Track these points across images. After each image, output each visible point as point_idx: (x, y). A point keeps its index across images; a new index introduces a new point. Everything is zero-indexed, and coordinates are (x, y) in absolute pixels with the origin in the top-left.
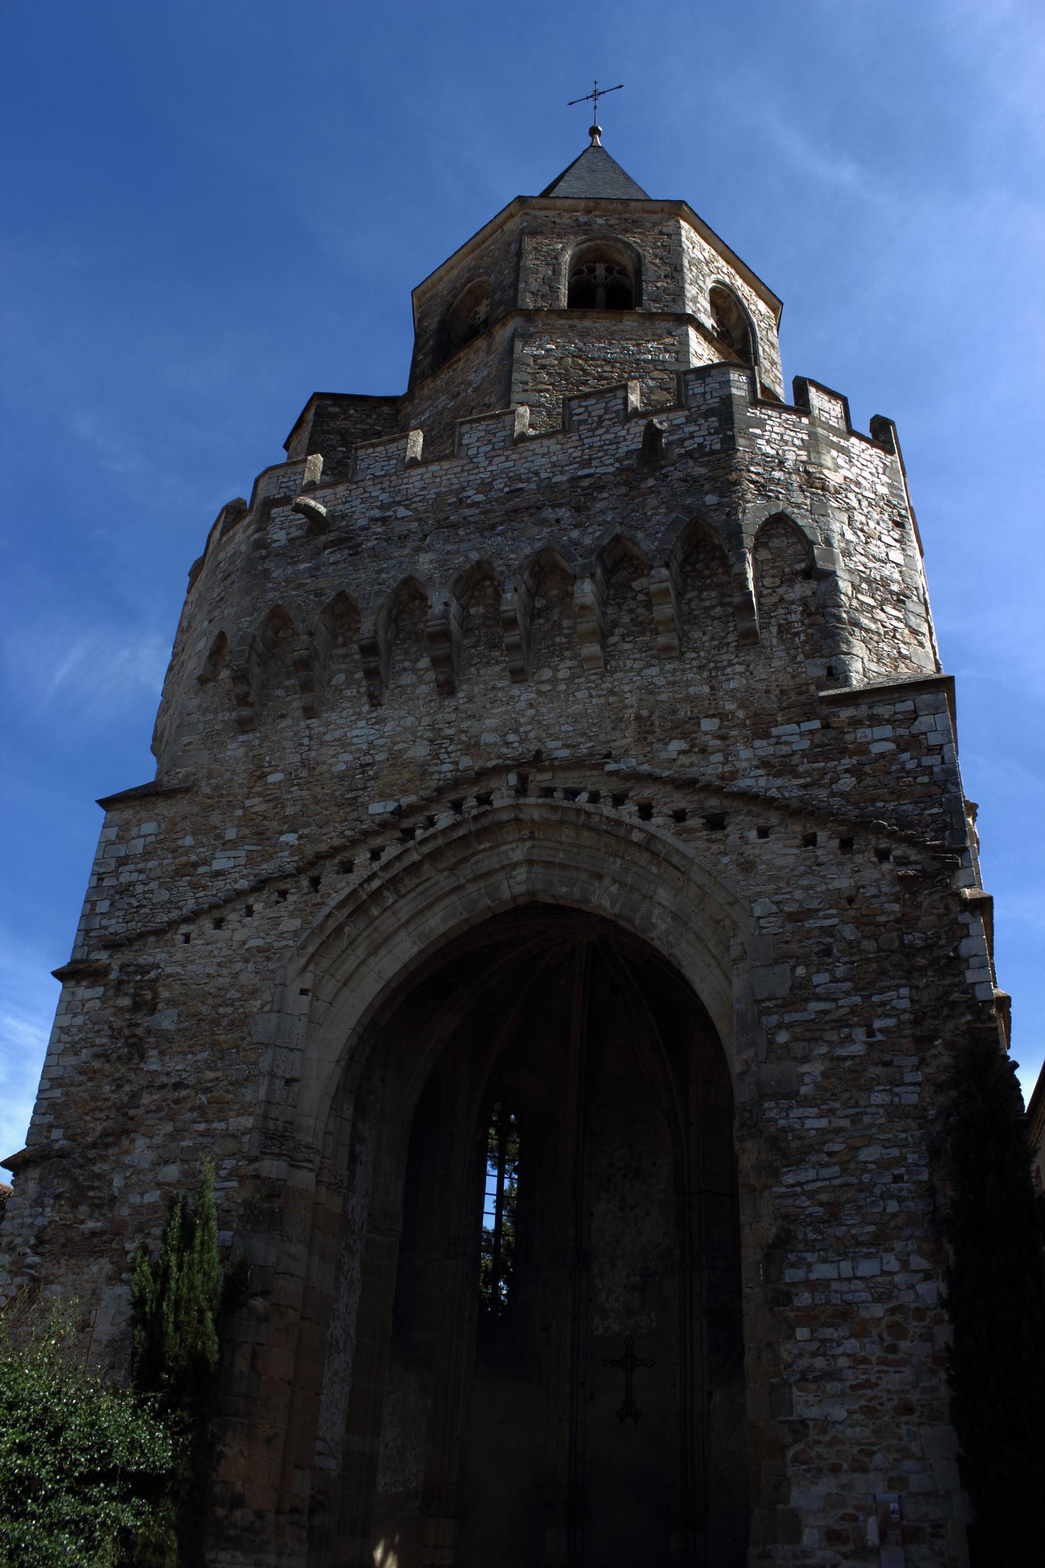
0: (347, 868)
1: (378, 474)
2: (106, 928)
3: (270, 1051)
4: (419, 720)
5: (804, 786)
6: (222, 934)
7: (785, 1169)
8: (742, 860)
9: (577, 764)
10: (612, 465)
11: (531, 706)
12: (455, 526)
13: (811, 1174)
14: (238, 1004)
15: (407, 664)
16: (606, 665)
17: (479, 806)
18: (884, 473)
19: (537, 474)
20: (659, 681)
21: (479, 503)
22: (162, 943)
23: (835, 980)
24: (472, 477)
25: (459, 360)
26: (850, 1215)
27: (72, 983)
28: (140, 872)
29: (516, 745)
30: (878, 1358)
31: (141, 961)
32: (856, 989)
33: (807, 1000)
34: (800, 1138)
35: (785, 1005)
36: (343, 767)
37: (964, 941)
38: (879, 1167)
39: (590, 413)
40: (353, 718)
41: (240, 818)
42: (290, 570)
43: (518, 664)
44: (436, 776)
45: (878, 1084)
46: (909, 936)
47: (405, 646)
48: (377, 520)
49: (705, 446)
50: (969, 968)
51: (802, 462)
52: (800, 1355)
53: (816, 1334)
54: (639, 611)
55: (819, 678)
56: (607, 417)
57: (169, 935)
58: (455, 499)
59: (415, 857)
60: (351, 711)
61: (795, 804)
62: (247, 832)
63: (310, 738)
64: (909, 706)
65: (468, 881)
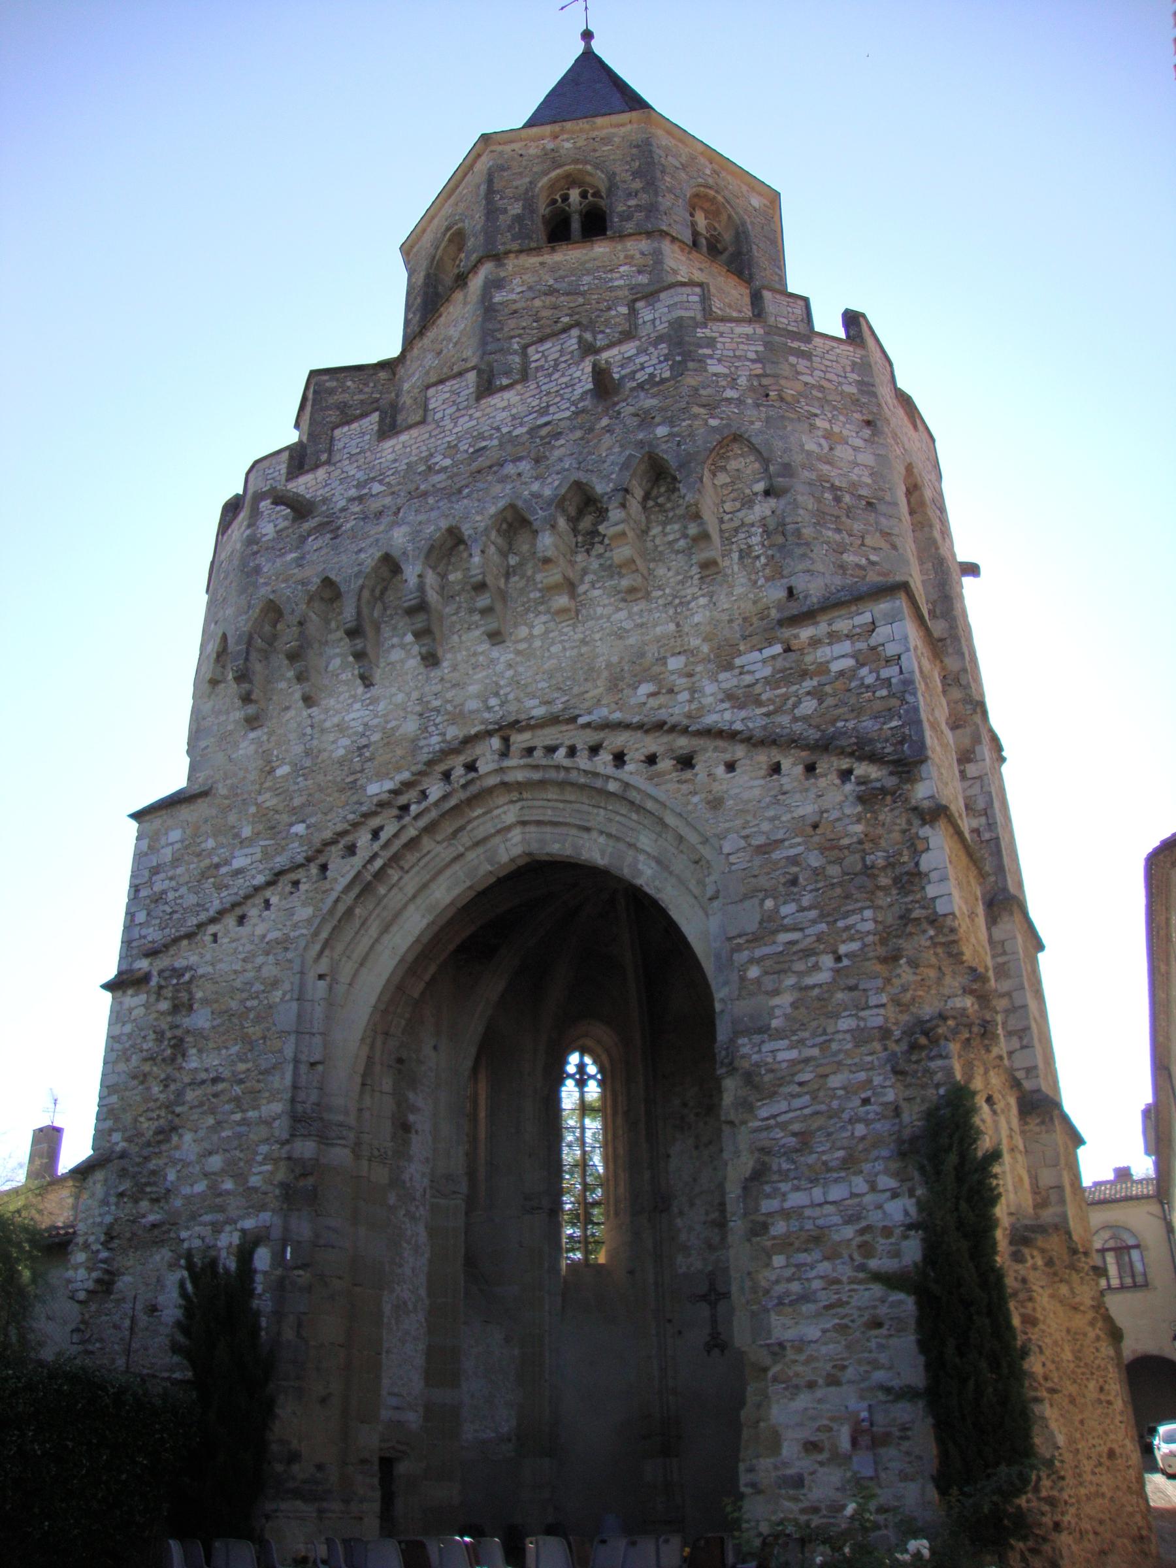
0: (351, 850)
1: (354, 452)
2: (145, 937)
4: (408, 695)
5: (767, 715)
6: (244, 931)
7: (759, 1104)
8: (711, 797)
9: (554, 720)
10: (568, 409)
11: (510, 666)
12: (425, 494)
13: (783, 1106)
14: (262, 996)
15: (395, 640)
16: (577, 615)
18: (853, 371)
19: (498, 429)
20: (628, 625)
21: (446, 468)
22: (194, 946)
23: (802, 909)
24: (440, 442)
25: (440, 316)
26: (820, 1142)
27: (119, 993)
28: (171, 879)
30: (849, 1277)
31: (177, 965)
32: (822, 916)
33: (775, 932)
34: (772, 1071)
35: (756, 939)
36: (341, 752)
37: (924, 856)
38: (848, 1092)
39: (546, 357)
41: (254, 815)
42: (279, 562)
43: (494, 626)
44: (426, 750)
45: (845, 1010)
46: (872, 857)
47: (393, 622)
49: (655, 376)
50: (929, 882)
51: (757, 376)
52: (777, 1282)
55: (780, 600)
56: (563, 359)
57: (199, 937)
58: (424, 468)
59: (412, 832)
60: (347, 695)
61: (759, 734)
62: (261, 827)
63: (312, 726)
64: (866, 618)
65: (467, 849)
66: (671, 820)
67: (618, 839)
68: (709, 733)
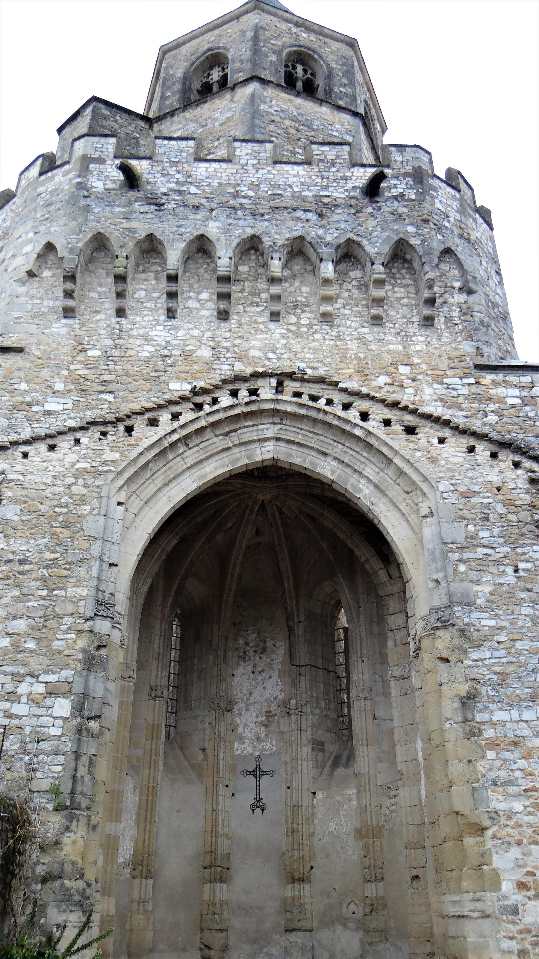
0: (153, 423)
3: (99, 542)
5: (466, 417)
8: (429, 456)
9: (321, 381)
13: (488, 654)
15: (192, 294)
17: (250, 395)
20: (370, 337)
29: (275, 361)
34: (479, 631)
36: (148, 355)
40: (153, 323)
41: (66, 377)
43: (275, 308)
48: (174, 191)
53: (500, 756)
54: (354, 291)
57: (10, 451)
59: (203, 423)
65: (235, 445)
66: (397, 461)
67: (347, 465)
68: (429, 417)
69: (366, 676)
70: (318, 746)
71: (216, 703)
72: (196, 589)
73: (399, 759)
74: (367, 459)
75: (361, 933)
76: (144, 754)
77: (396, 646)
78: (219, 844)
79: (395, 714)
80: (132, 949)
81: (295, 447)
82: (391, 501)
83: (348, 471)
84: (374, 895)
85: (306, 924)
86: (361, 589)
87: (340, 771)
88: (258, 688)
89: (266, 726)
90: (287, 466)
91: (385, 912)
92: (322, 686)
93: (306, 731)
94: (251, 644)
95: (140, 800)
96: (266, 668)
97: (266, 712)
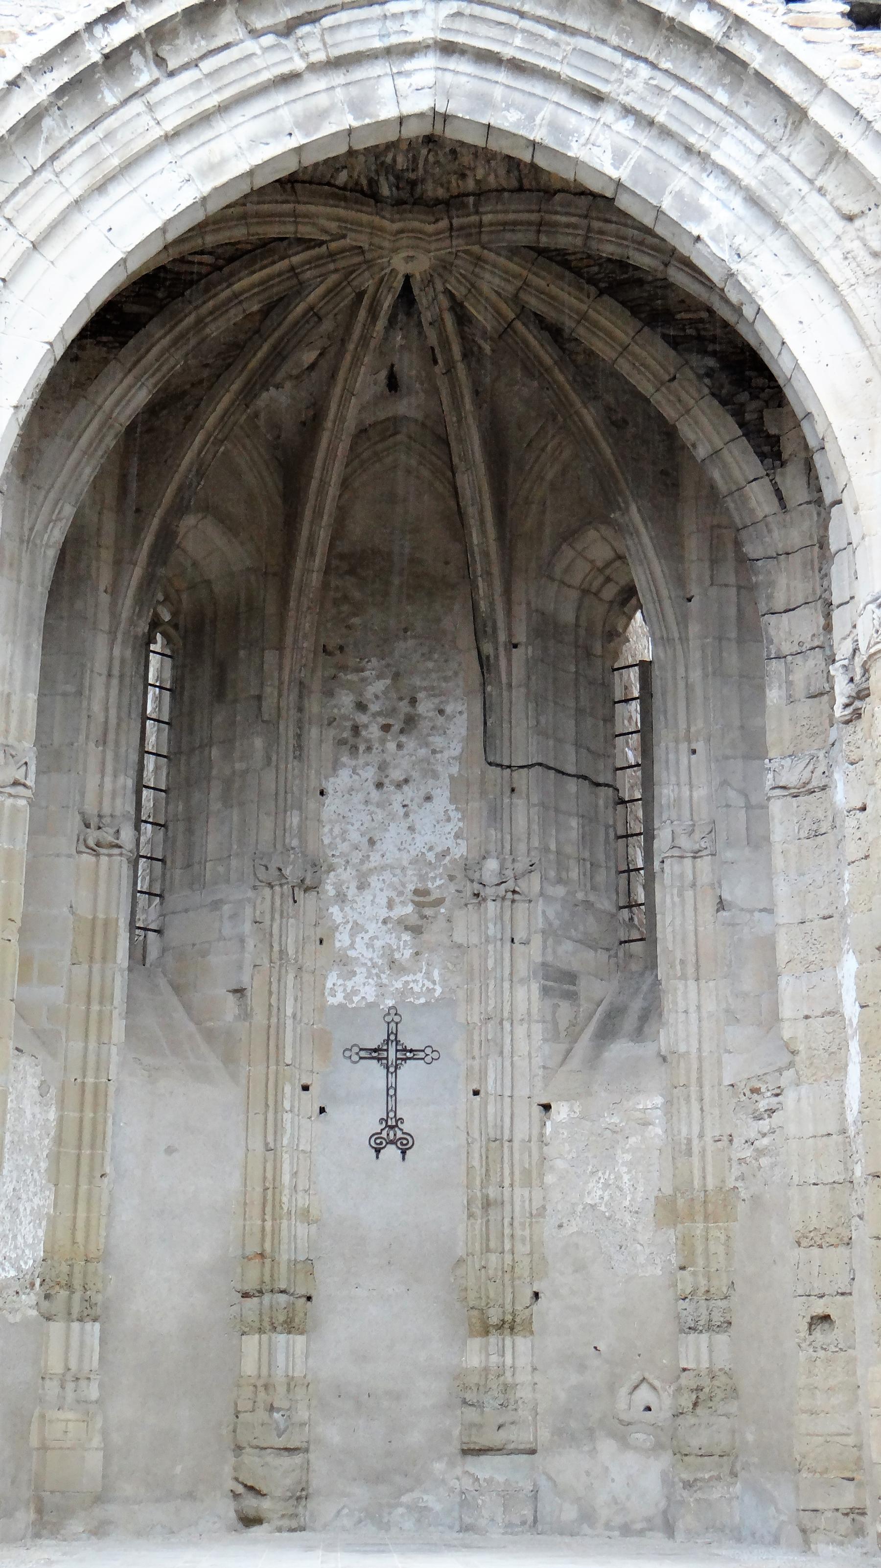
66: (821, 112)
67: (665, 133)
69: (700, 793)
70: (560, 983)
71: (273, 866)
72: (211, 549)
73: (787, 1011)
74: (727, 111)
75: (665, 1460)
76: (69, 1001)
77: (791, 700)
78: (284, 1233)
79: (782, 889)
80: (46, 1495)
81: (502, 76)
82: (798, 246)
83: (668, 151)
84: (705, 1364)
85: (521, 1436)
86: (694, 547)
87: (620, 1050)
88: (393, 827)
89: (416, 931)
90: (476, 139)
91: (733, 1407)
92: (574, 823)
93: (526, 943)
94: (374, 707)
95: (61, 1120)
96: (415, 775)
97: (416, 892)
